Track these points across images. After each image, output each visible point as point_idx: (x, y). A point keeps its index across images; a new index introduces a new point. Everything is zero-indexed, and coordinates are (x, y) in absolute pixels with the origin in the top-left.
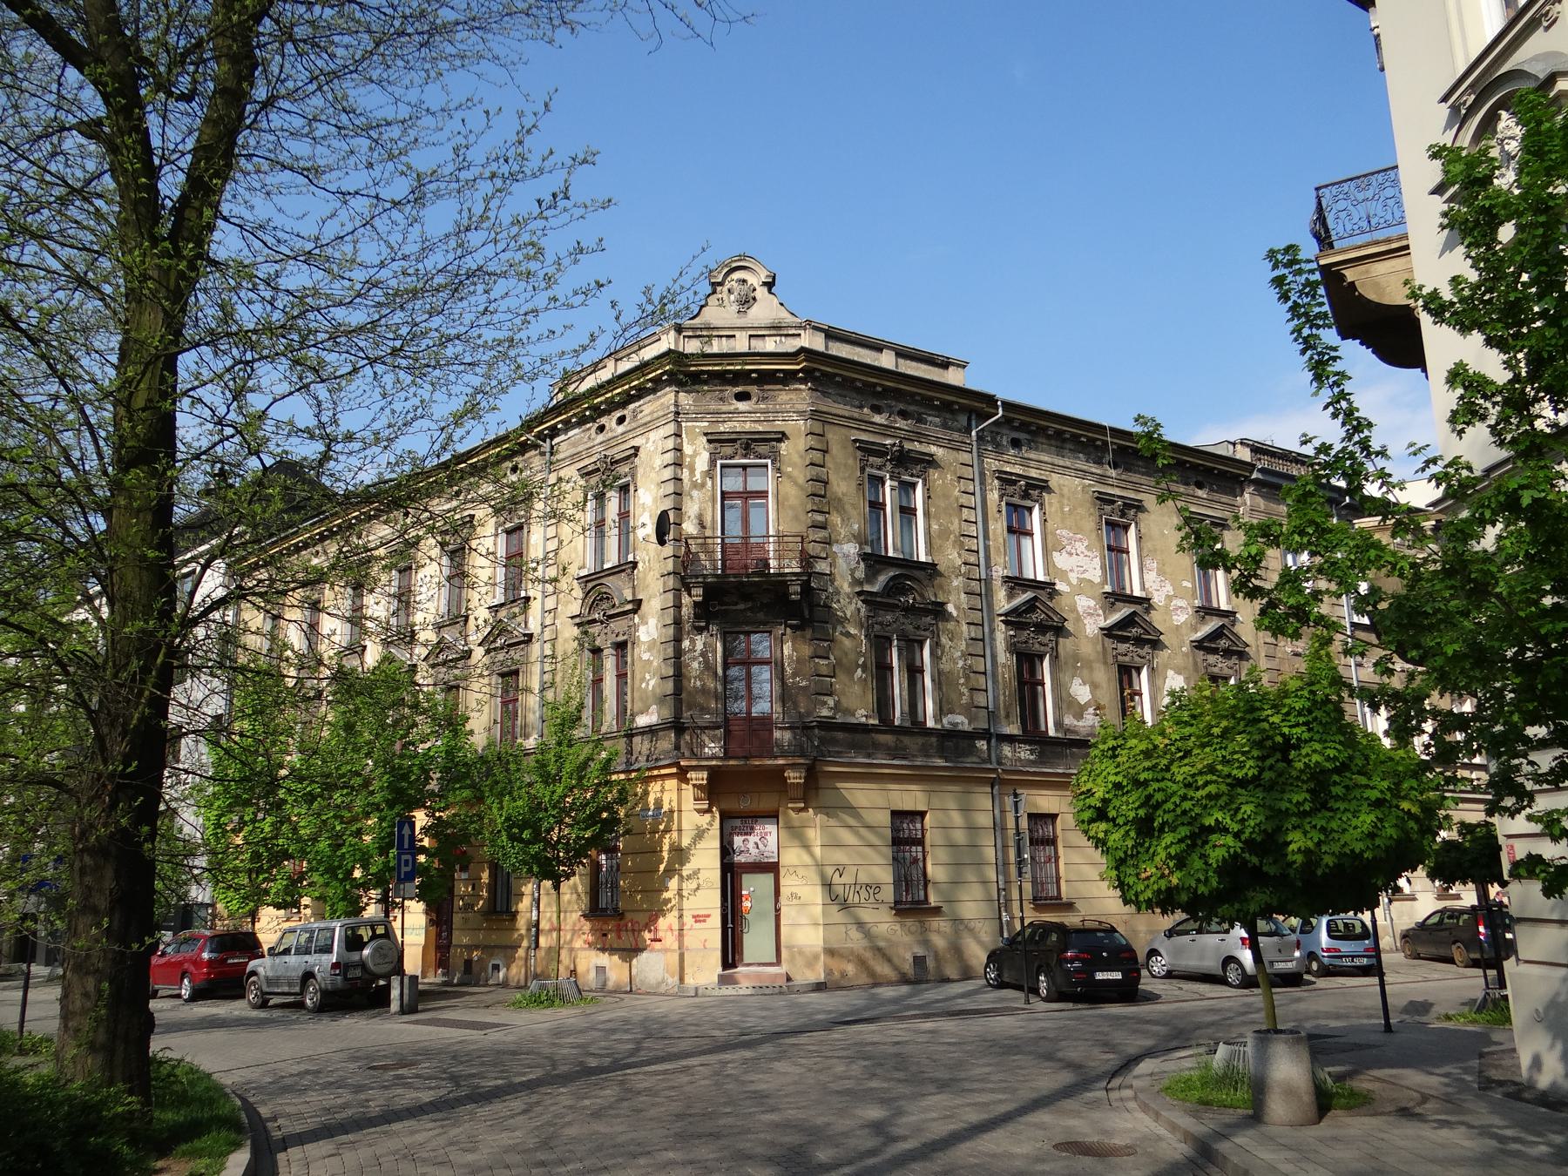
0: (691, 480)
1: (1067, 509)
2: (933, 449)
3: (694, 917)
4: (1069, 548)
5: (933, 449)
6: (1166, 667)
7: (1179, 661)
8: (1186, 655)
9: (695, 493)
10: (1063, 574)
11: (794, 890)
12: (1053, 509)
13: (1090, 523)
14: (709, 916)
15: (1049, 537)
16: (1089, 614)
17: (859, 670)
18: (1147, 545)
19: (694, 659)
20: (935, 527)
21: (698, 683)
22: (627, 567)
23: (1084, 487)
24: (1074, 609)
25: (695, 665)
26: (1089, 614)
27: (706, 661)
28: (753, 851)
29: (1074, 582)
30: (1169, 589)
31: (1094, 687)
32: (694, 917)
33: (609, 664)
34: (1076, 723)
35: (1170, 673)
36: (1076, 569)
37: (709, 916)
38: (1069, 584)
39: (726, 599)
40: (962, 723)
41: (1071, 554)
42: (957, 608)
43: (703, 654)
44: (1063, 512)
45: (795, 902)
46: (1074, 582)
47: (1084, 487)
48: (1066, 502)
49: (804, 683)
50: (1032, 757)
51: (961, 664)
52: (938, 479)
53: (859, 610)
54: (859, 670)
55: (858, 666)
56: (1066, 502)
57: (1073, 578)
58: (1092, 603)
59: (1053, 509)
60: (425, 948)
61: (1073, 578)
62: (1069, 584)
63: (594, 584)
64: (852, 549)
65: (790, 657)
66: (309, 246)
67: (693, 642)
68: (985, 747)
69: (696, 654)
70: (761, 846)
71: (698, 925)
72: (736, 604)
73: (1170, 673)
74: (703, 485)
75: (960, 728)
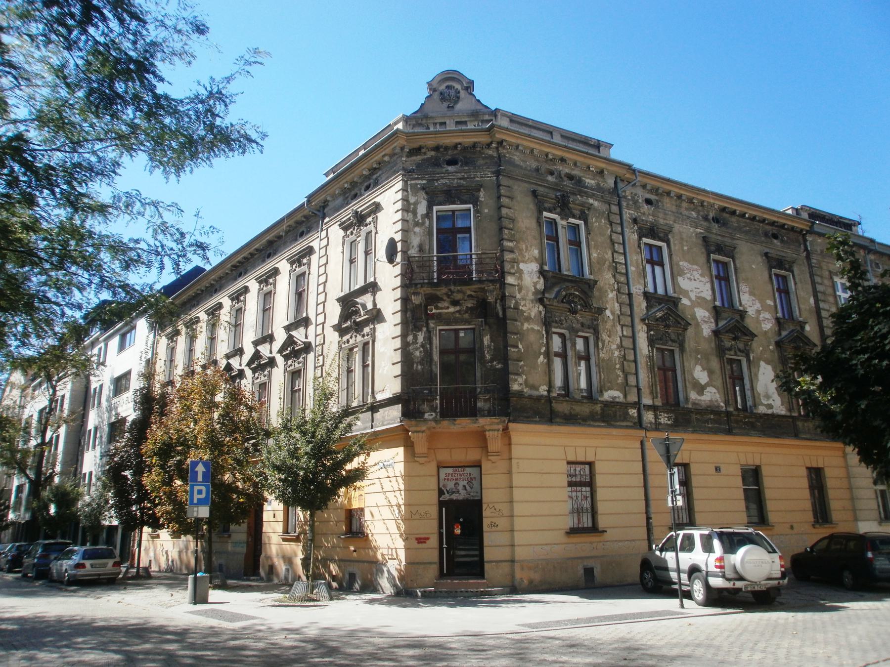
0: (414, 220)
1: (685, 248)
2: (591, 201)
3: (417, 539)
4: (688, 275)
5: (591, 201)
6: (759, 359)
7: (767, 355)
8: (772, 351)
9: (417, 229)
10: (686, 293)
11: (493, 520)
12: (677, 248)
13: (702, 259)
14: (428, 539)
15: (675, 267)
16: (705, 322)
17: (542, 357)
18: (742, 275)
19: (417, 349)
20: (595, 255)
21: (419, 367)
22: (372, 288)
23: (697, 234)
24: (694, 317)
25: (417, 353)
26: (705, 322)
27: (425, 351)
28: (463, 492)
29: (693, 298)
30: (758, 305)
31: (711, 373)
32: (417, 539)
33: (357, 357)
34: (699, 398)
35: (762, 363)
36: (695, 290)
37: (428, 539)
38: (690, 299)
39: (439, 305)
40: (619, 397)
41: (690, 279)
42: (613, 313)
43: (423, 346)
44: (683, 250)
45: (494, 529)
46: (693, 298)
47: (697, 234)
48: (685, 243)
49: (499, 366)
50: (669, 422)
51: (616, 353)
52: (596, 222)
53: (540, 312)
54: (542, 357)
55: (540, 354)
56: (685, 243)
57: (693, 296)
58: (707, 314)
59: (677, 248)
60: (246, 555)
61: (693, 296)
62: (690, 299)
63: (348, 303)
64: (534, 267)
65: (489, 346)
66: (575, 515)
67: (415, 337)
68: (636, 415)
69: (418, 345)
70: (468, 488)
71: (421, 546)
72: (448, 308)
73: (762, 363)
74: (423, 224)
75: (617, 400)
